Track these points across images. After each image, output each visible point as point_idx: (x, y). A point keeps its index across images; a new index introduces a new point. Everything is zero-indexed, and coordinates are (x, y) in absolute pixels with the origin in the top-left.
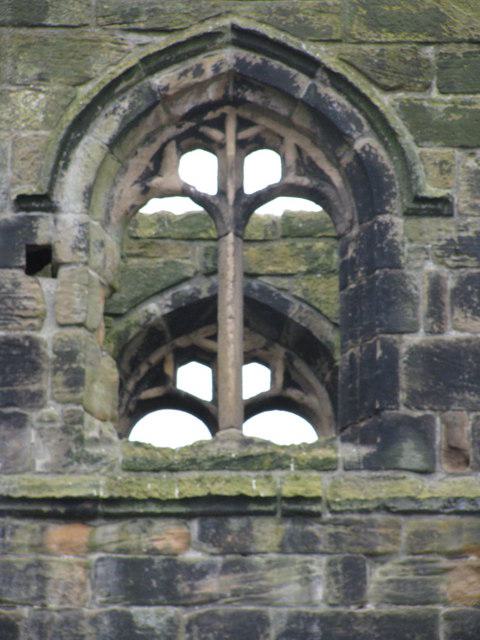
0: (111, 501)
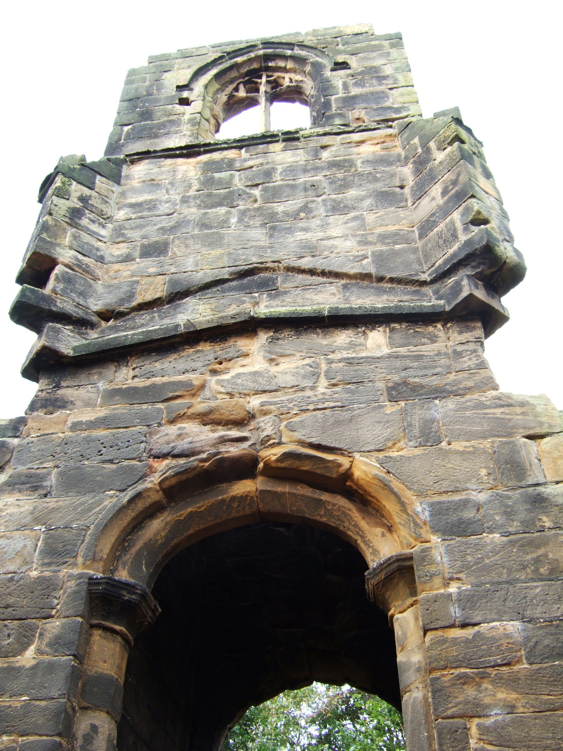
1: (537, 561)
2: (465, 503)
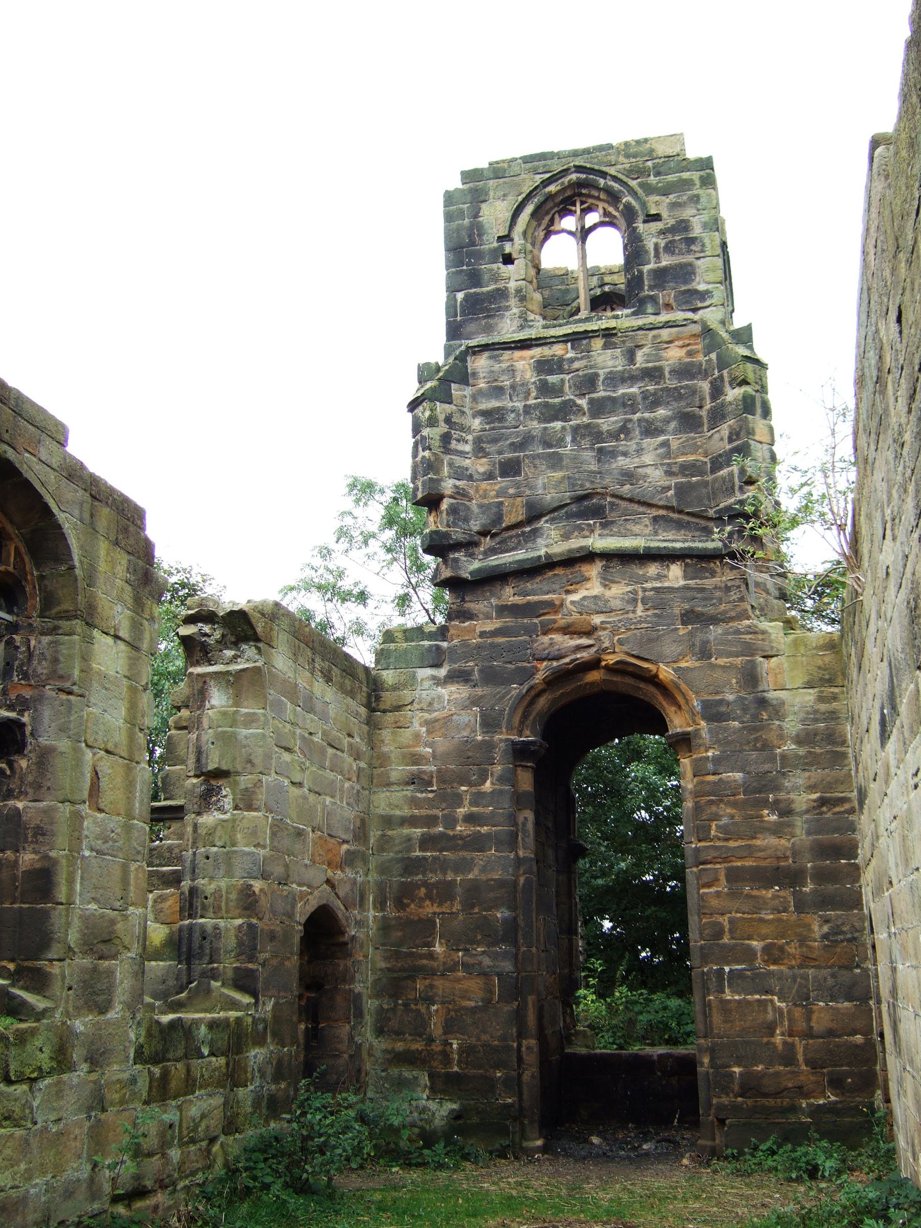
0: (537, 339)
1: (756, 740)
2: (721, 702)
